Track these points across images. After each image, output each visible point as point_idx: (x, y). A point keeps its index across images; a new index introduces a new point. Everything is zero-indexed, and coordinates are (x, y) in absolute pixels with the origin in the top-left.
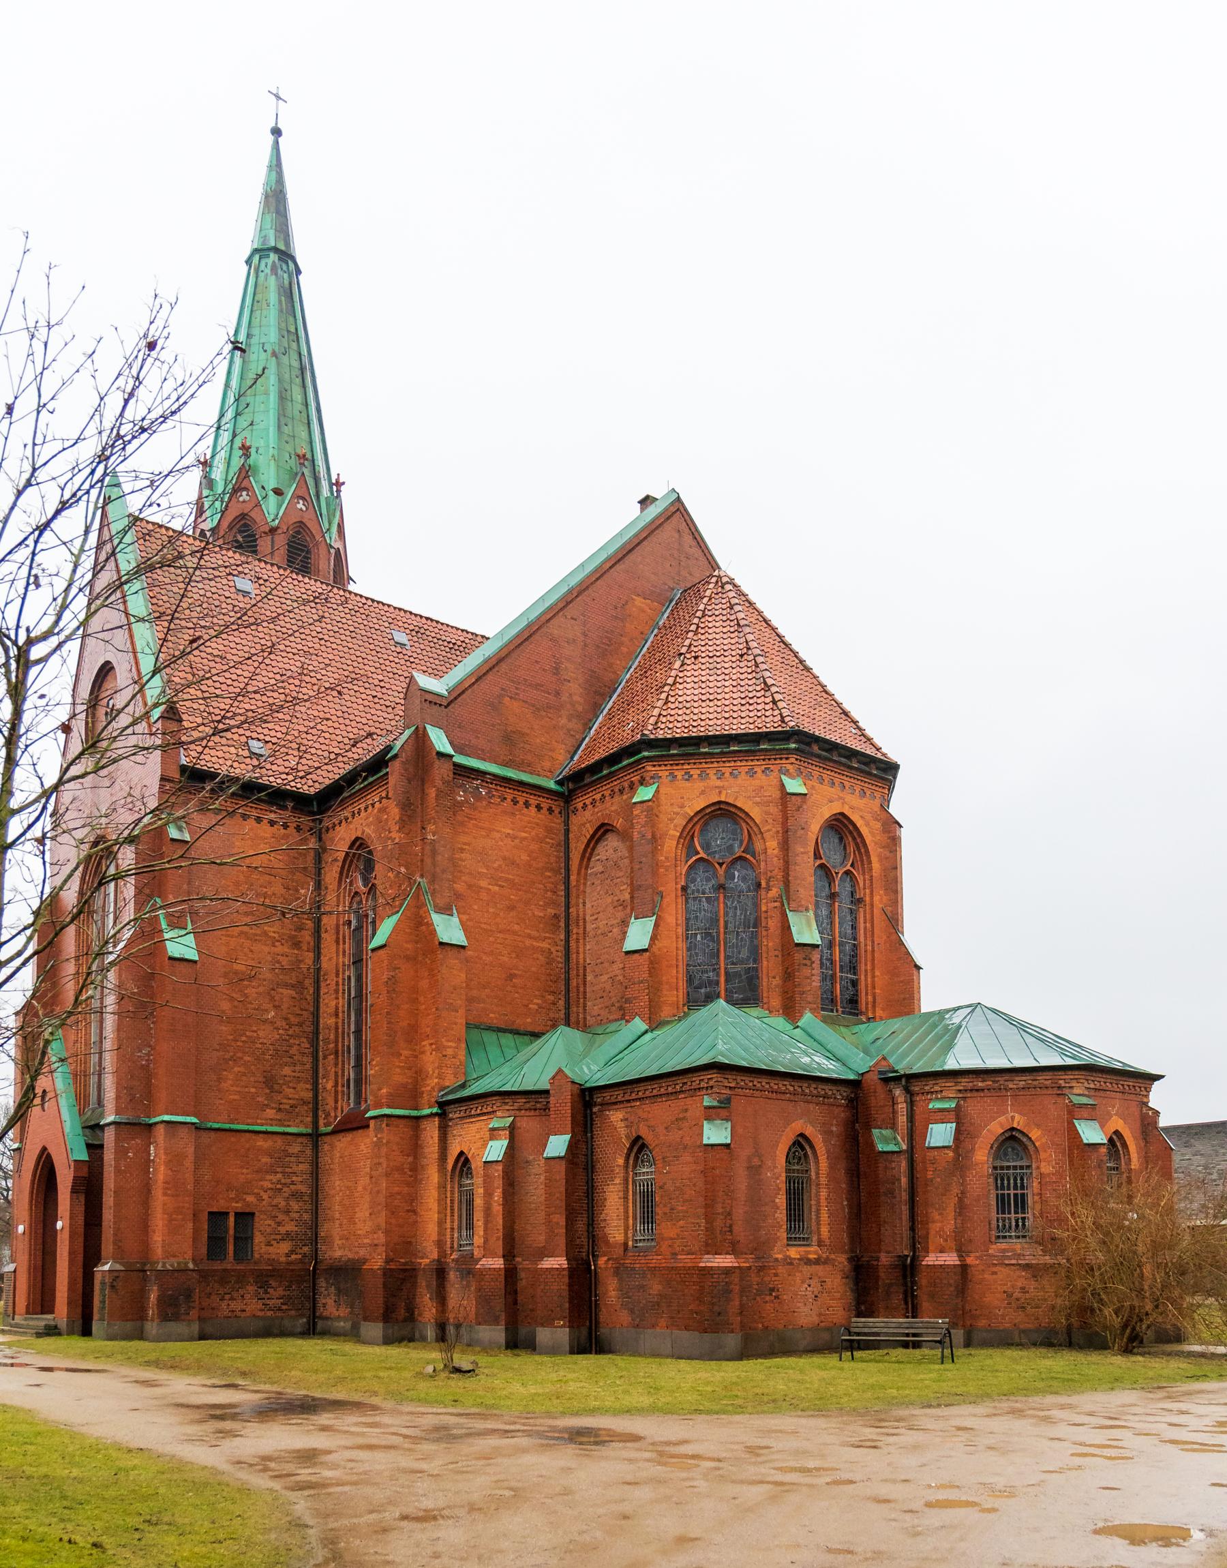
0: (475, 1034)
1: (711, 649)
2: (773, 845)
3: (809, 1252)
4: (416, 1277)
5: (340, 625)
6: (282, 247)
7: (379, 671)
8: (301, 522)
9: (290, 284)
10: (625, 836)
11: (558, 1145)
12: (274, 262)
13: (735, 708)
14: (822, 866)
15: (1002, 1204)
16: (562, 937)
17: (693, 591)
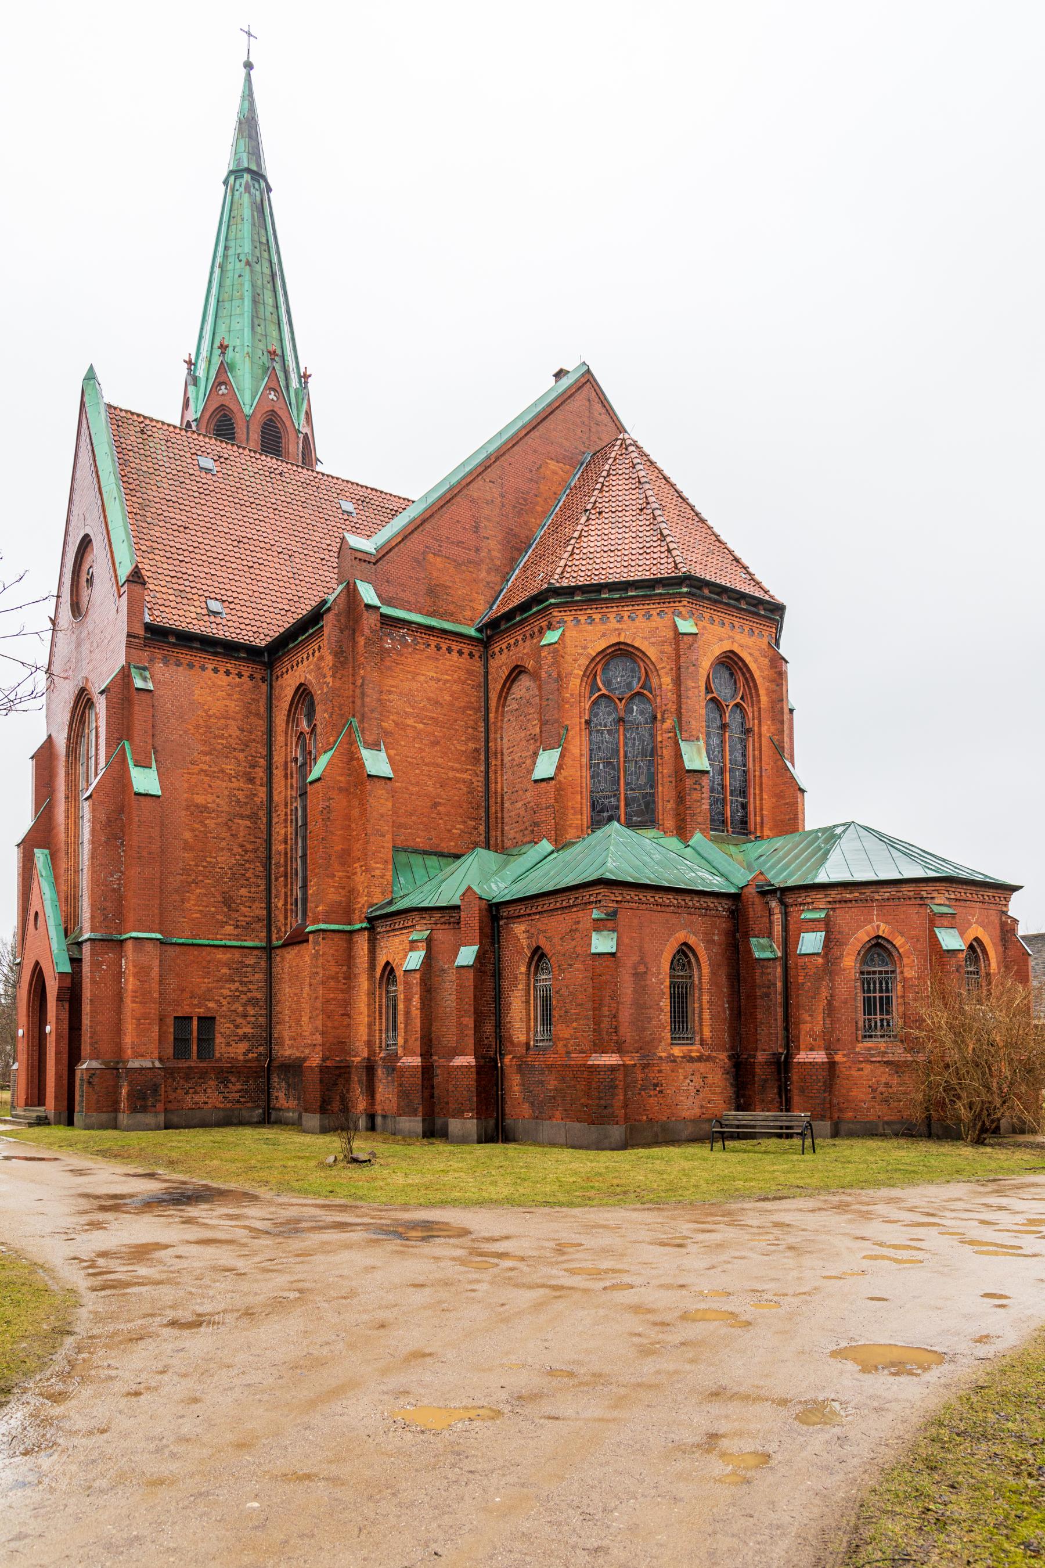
0: (402, 857)
1: (614, 505)
2: (667, 681)
3: (691, 1051)
4: (349, 1073)
5: (293, 496)
6: (254, 168)
7: (327, 536)
8: (273, 411)
9: (262, 200)
10: (535, 676)
11: (467, 955)
12: (247, 182)
13: (633, 558)
14: (713, 700)
15: (869, 1006)
16: (482, 769)
17: (601, 454)
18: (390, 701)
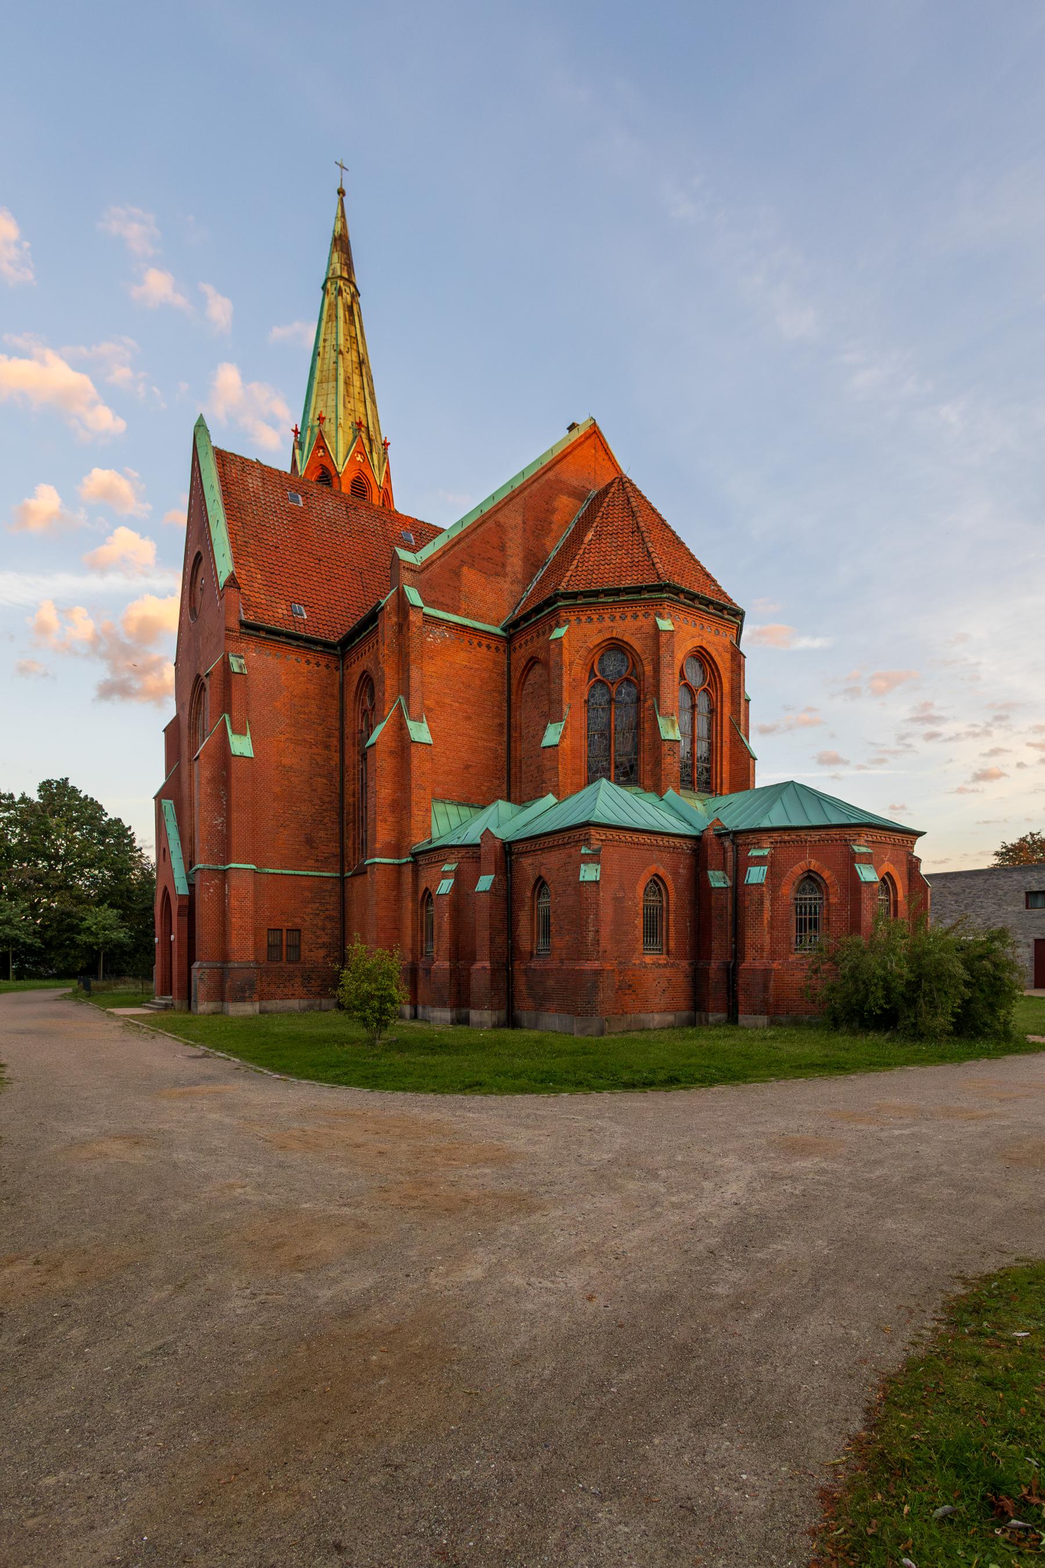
2: (648, 669)
6: (345, 275)
11: (485, 883)
16: (505, 739)
18: (431, 683)
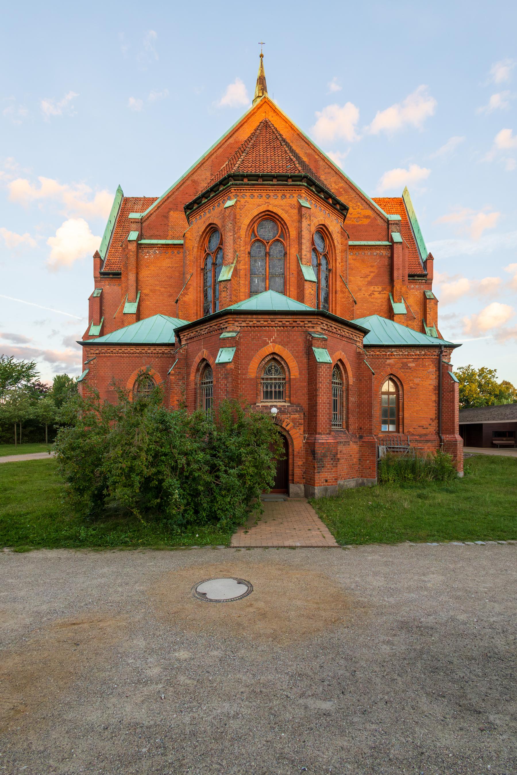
18: (147, 281)
